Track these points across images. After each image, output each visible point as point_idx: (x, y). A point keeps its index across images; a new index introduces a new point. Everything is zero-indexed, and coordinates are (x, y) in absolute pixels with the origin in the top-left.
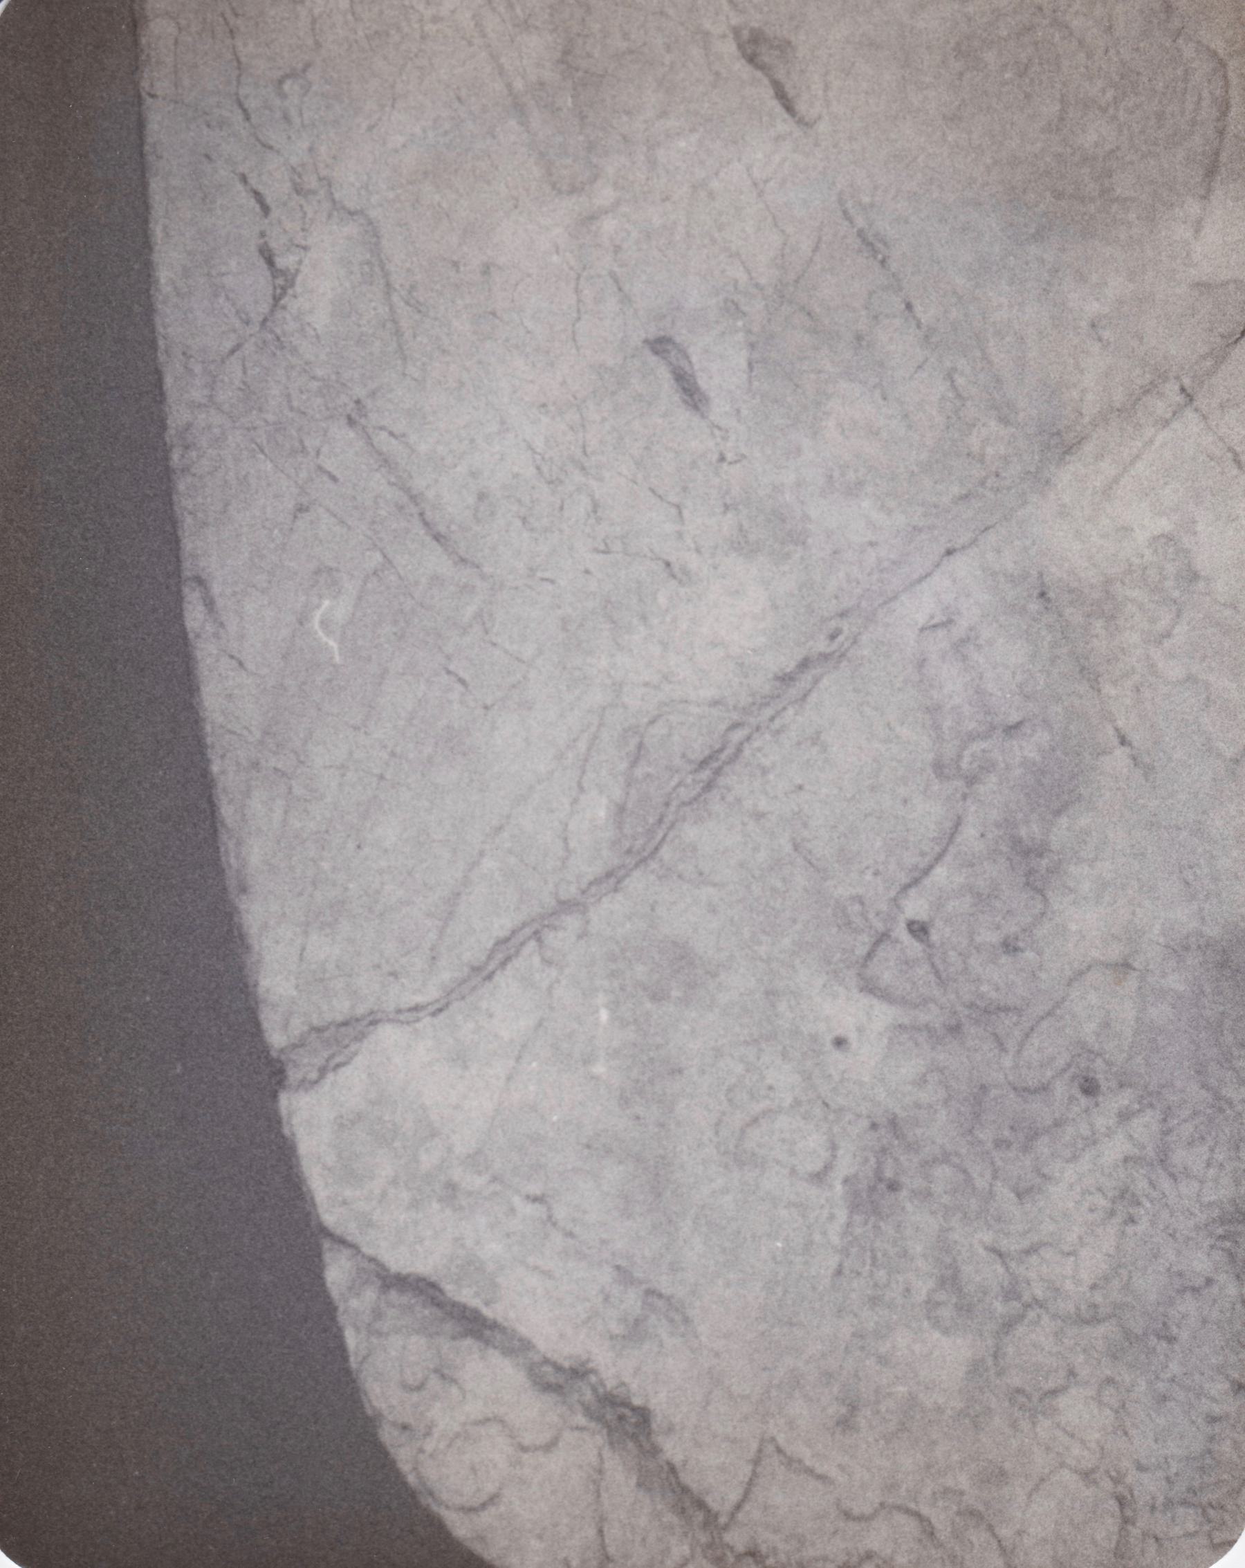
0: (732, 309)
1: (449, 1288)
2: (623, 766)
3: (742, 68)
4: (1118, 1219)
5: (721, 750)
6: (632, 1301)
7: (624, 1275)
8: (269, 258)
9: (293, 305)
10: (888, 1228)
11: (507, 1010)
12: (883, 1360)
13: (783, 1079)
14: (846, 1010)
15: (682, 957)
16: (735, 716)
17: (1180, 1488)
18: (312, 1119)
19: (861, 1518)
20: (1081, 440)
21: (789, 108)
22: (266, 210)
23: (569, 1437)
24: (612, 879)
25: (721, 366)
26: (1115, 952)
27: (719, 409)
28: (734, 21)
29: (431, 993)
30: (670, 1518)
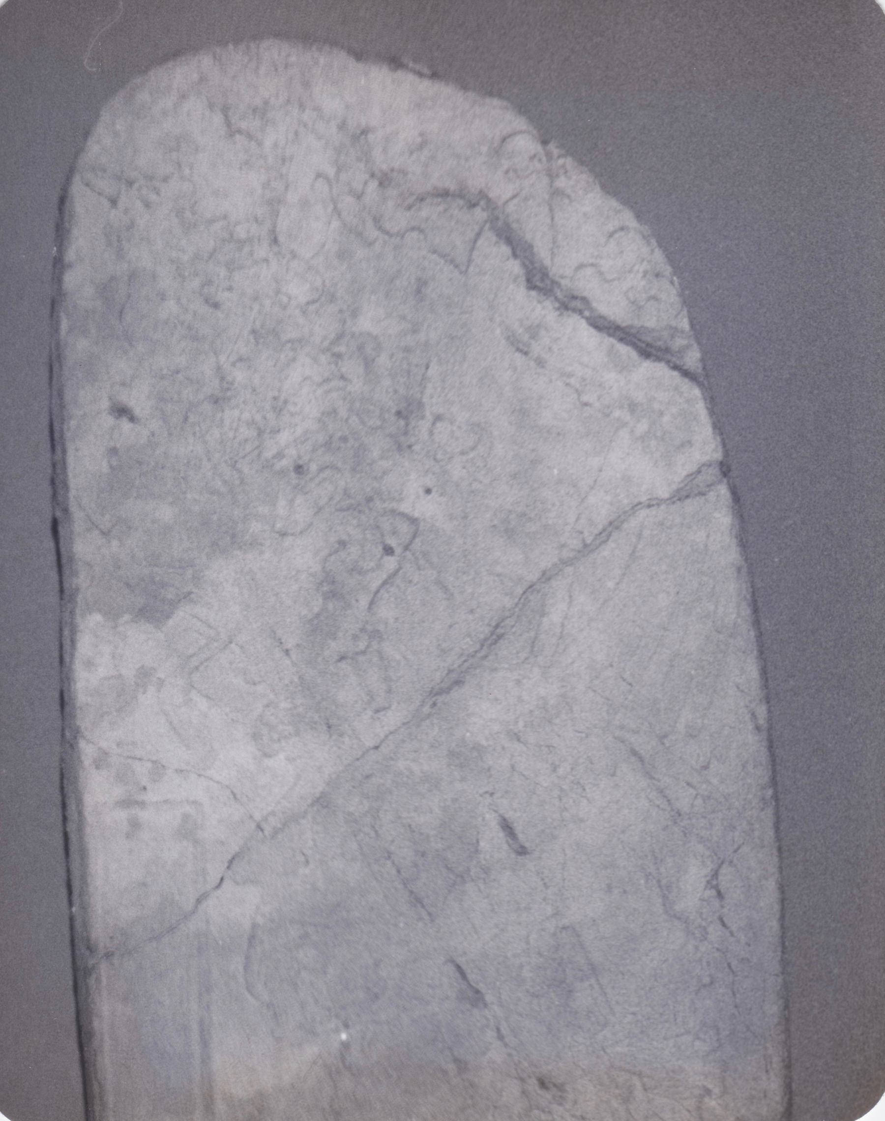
0: (486, 870)
1: (634, 354)
2: (542, 636)
3: (481, 986)
4: (282, 398)
5: (491, 645)
6: (536, 349)
7: (540, 363)
8: (720, 895)
9: (707, 871)
10: (402, 391)
11: (601, 505)
12: (403, 318)
13: (457, 471)
14: (428, 509)
15: (510, 533)
16: (486, 663)
17: (246, 249)
18: (705, 446)
19: (413, 229)
20: (312, 805)
21: (459, 968)
22: (721, 920)
23: (568, 272)
24: (546, 577)
25: (492, 842)
26: (288, 541)
27: (492, 819)
28: (486, 1012)
29: (643, 513)
30: (515, 226)
